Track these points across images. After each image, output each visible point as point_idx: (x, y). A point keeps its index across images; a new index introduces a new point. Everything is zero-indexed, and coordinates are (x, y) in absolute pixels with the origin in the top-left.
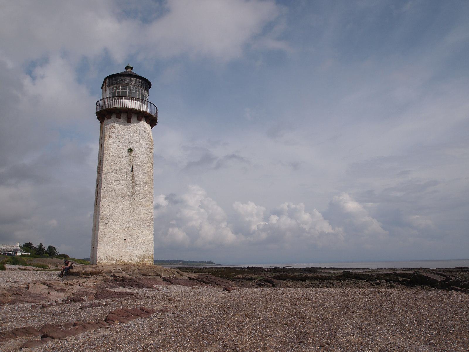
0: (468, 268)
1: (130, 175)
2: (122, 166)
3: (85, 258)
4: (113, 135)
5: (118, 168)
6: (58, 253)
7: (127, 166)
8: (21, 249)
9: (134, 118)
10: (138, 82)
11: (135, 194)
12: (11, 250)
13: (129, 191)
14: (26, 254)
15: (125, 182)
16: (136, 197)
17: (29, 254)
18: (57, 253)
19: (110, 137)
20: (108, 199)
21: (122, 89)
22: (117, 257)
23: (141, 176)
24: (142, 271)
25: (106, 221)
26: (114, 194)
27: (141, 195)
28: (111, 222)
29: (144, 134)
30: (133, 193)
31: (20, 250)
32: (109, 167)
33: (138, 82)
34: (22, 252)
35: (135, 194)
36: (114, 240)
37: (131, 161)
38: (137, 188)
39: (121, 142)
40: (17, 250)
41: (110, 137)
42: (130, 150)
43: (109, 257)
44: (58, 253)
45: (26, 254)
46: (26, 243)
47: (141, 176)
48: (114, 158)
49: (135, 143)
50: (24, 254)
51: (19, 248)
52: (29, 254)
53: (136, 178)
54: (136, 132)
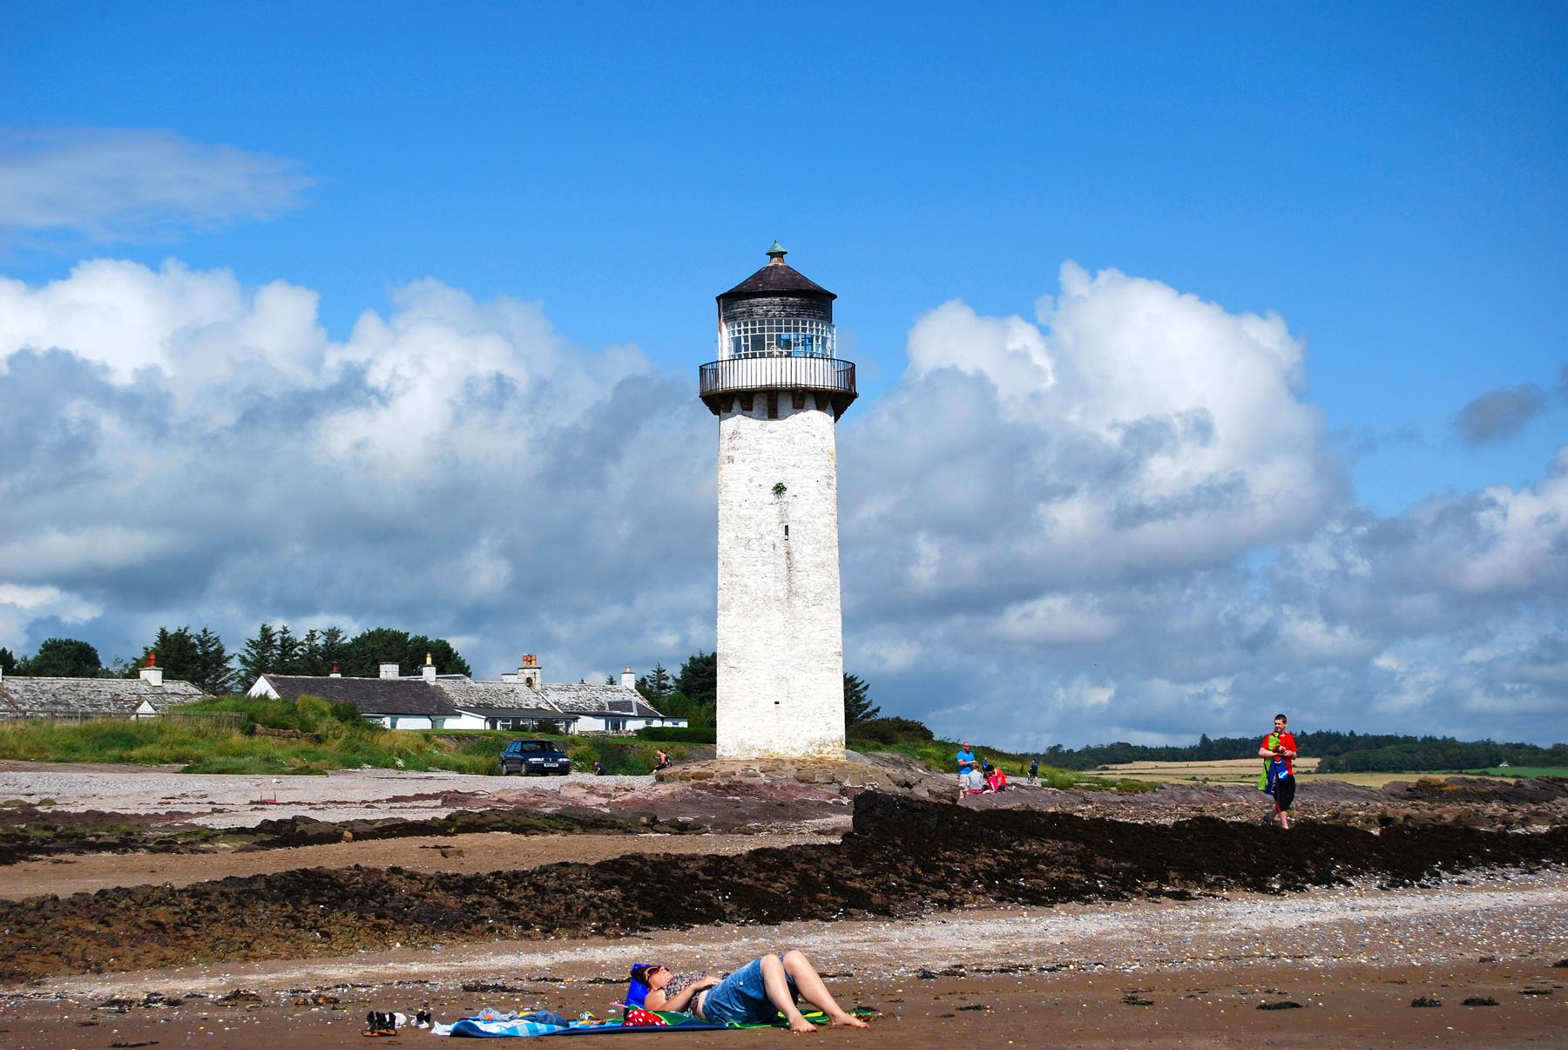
0: (1559, 755)
1: (782, 551)
2: (763, 530)
3: (1352, 733)
4: (737, 455)
5: (751, 535)
6: (877, 710)
7: (774, 527)
8: (644, 702)
9: (785, 404)
10: (791, 306)
11: (796, 594)
12: (602, 707)
13: (780, 588)
14: (668, 724)
15: (770, 567)
16: (797, 602)
17: (684, 724)
18: (868, 715)
19: (731, 460)
20: (734, 611)
21: (753, 331)
22: (760, 743)
23: (808, 549)
24: (803, 773)
25: (732, 662)
26: (746, 599)
27: (808, 595)
28: (743, 665)
29: (811, 441)
30: (791, 593)
31: (639, 706)
32: (732, 536)
33: (791, 306)
34: (647, 716)
35: (796, 594)
36: (753, 705)
37: (783, 514)
38: (800, 580)
39: (756, 469)
40: (626, 705)
41: (731, 460)
42: (779, 489)
43: (742, 742)
44: (877, 710)
45: (668, 724)
46: (697, 656)
47: (808, 549)
48: (743, 512)
49: (790, 469)
50: (656, 724)
51: (637, 699)
52: (684, 724)
53: (797, 556)
54: (791, 440)
